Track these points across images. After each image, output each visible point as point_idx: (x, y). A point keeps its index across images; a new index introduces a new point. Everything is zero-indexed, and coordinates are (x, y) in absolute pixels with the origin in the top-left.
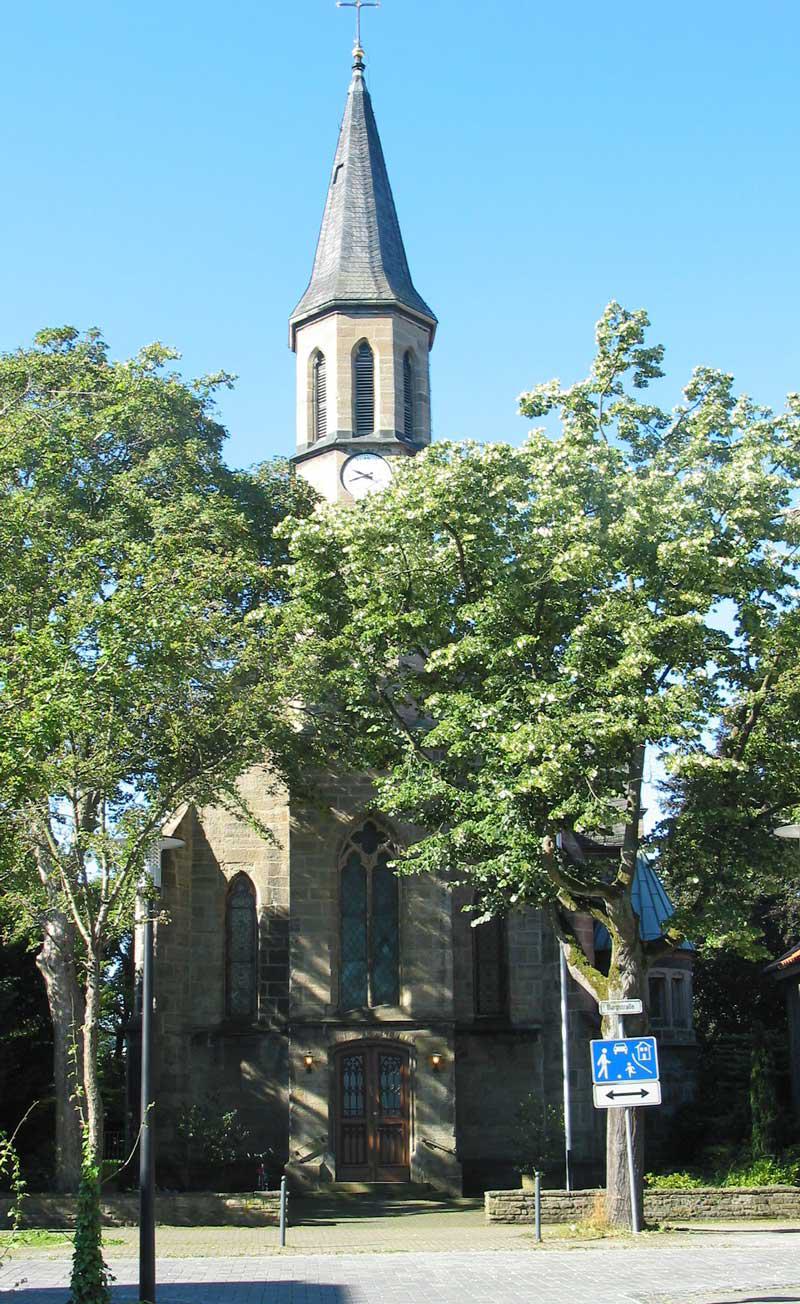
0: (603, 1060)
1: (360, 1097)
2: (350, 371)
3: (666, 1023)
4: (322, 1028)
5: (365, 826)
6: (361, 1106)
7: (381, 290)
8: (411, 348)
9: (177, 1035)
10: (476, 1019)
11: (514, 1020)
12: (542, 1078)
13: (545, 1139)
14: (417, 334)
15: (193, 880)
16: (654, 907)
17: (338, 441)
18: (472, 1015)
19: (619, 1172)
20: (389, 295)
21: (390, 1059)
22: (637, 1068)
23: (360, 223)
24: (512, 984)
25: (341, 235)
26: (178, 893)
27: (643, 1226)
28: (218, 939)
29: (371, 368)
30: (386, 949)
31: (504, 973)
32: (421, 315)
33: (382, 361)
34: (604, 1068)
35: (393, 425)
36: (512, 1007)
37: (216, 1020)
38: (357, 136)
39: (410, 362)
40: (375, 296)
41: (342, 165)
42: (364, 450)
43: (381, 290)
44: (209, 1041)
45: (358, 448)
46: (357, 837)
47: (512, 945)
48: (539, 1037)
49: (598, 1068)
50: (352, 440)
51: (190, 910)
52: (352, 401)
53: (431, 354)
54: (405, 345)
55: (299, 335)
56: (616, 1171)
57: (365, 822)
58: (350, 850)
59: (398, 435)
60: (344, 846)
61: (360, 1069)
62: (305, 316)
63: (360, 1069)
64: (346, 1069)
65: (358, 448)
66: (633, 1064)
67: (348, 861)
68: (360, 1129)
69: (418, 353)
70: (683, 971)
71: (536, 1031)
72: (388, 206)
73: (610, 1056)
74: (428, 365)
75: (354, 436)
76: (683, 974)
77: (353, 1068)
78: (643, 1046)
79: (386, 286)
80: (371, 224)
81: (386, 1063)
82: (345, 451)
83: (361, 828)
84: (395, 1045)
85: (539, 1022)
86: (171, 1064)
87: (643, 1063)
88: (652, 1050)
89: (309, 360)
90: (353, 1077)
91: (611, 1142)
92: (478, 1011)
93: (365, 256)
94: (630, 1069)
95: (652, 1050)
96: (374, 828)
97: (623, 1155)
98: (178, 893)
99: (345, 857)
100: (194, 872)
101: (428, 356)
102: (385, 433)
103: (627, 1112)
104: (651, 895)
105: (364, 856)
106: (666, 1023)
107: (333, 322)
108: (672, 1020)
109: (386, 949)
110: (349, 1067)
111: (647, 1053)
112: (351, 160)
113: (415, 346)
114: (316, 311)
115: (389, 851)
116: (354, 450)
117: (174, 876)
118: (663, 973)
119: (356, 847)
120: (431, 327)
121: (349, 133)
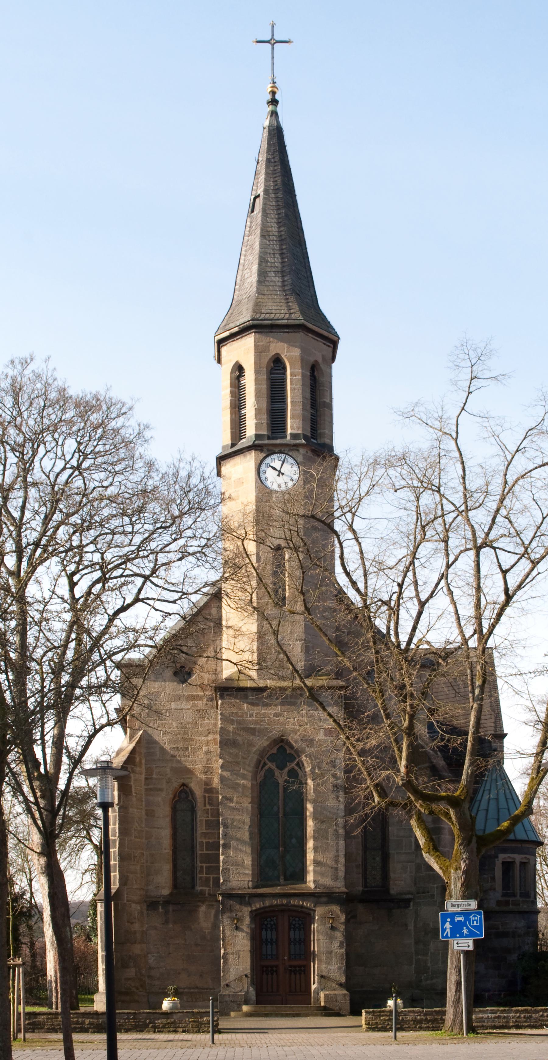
0: (448, 925)
1: (274, 946)
2: (265, 382)
3: (514, 895)
4: (245, 897)
5: (278, 749)
6: (274, 953)
7: (292, 311)
8: (316, 361)
9: (136, 903)
10: (363, 891)
11: (393, 892)
12: (413, 934)
13: (33, 774)
14: (321, 349)
15: (146, 789)
16: (508, 809)
17: (256, 442)
18: (361, 889)
19: (456, 995)
20: (297, 317)
21: (297, 919)
22: (470, 931)
23: (273, 249)
24: (391, 866)
25: (257, 261)
26: (134, 799)
27: (472, 1029)
28: (165, 834)
29: (284, 381)
30: (294, 841)
31: (385, 858)
32: (325, 333)
33: (292, 374)
34: (448, 930)
35: (301, 429)
36: (391, 882)
37: (166, 892)
38: (271, 168)
39: (316, 373)
40: (287, 316)
41: (258, 196)
42: (277, 450)
43: (292, 311)
44: (160, 907)
45: (270, 448)
46: (272, 758)
47: (391, 838)
48: (412, 904)
49: (444, 930)
50: (266, 442)
51: (144, 812)
52: (267, 409)
53: (334, 365)
54: (312, 359)
55: (224, 350)
56: (453, 994)
57: (277, 747)
58: (266, 768)
59: (305, 437)
60: (261, 766)
61: (274, 927)
62: (227, 334)
63: (274, 927)
64: (264, 926)
65: (270, 448)
66: (467, 928)
67: (265, 776)
68: (275, 969)
69: (323, 367)
70: (528, 856)
71: (409, 901)
72: (294, 206)
73: (452, 923)
74: (330, 376)
75: (269, 438)
76: (529, 859)
77: (269, 926)
78: (475, 916)
79: (295, 307)
80: (284, 251)
81: (294, 922)
82: (262, 451)
83: (275, 751)
84: (300, 909)
85: (412, 894)
86: (132, 923)
87: (474, 927)
88: (481, 919)
89: (232, 373)
90: (269, 932)
91: (451, 974)
92: (365, 885)
93: (278, 280)
94: (465, 931)
95: (481, 919)
96: (285, 750)
97: (458, 983)
98: (134, 799)
99: (262, 773)
100: (146, 784)
101: (331, 368)
102: (294, 436)
103: (462, 955)
104: (507, 799)
105: (277, 772)
106: (514, 895)
107: (249, 341)
108: (518, 891)
109: (294, 841)
110: (266, 925)
111: (477, 921)
112: (266, 191)
113: (320, 361)
114: (236, 329)
115: (296, 768)
116: (268, 450)
117: (131, 787)
118: (513, 858)
119: (270, 765)
120: (339, 338)
121: (264, 166)
